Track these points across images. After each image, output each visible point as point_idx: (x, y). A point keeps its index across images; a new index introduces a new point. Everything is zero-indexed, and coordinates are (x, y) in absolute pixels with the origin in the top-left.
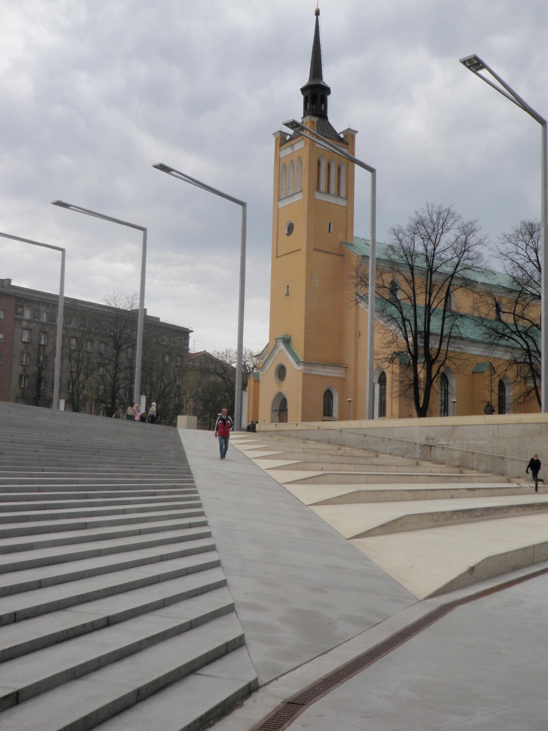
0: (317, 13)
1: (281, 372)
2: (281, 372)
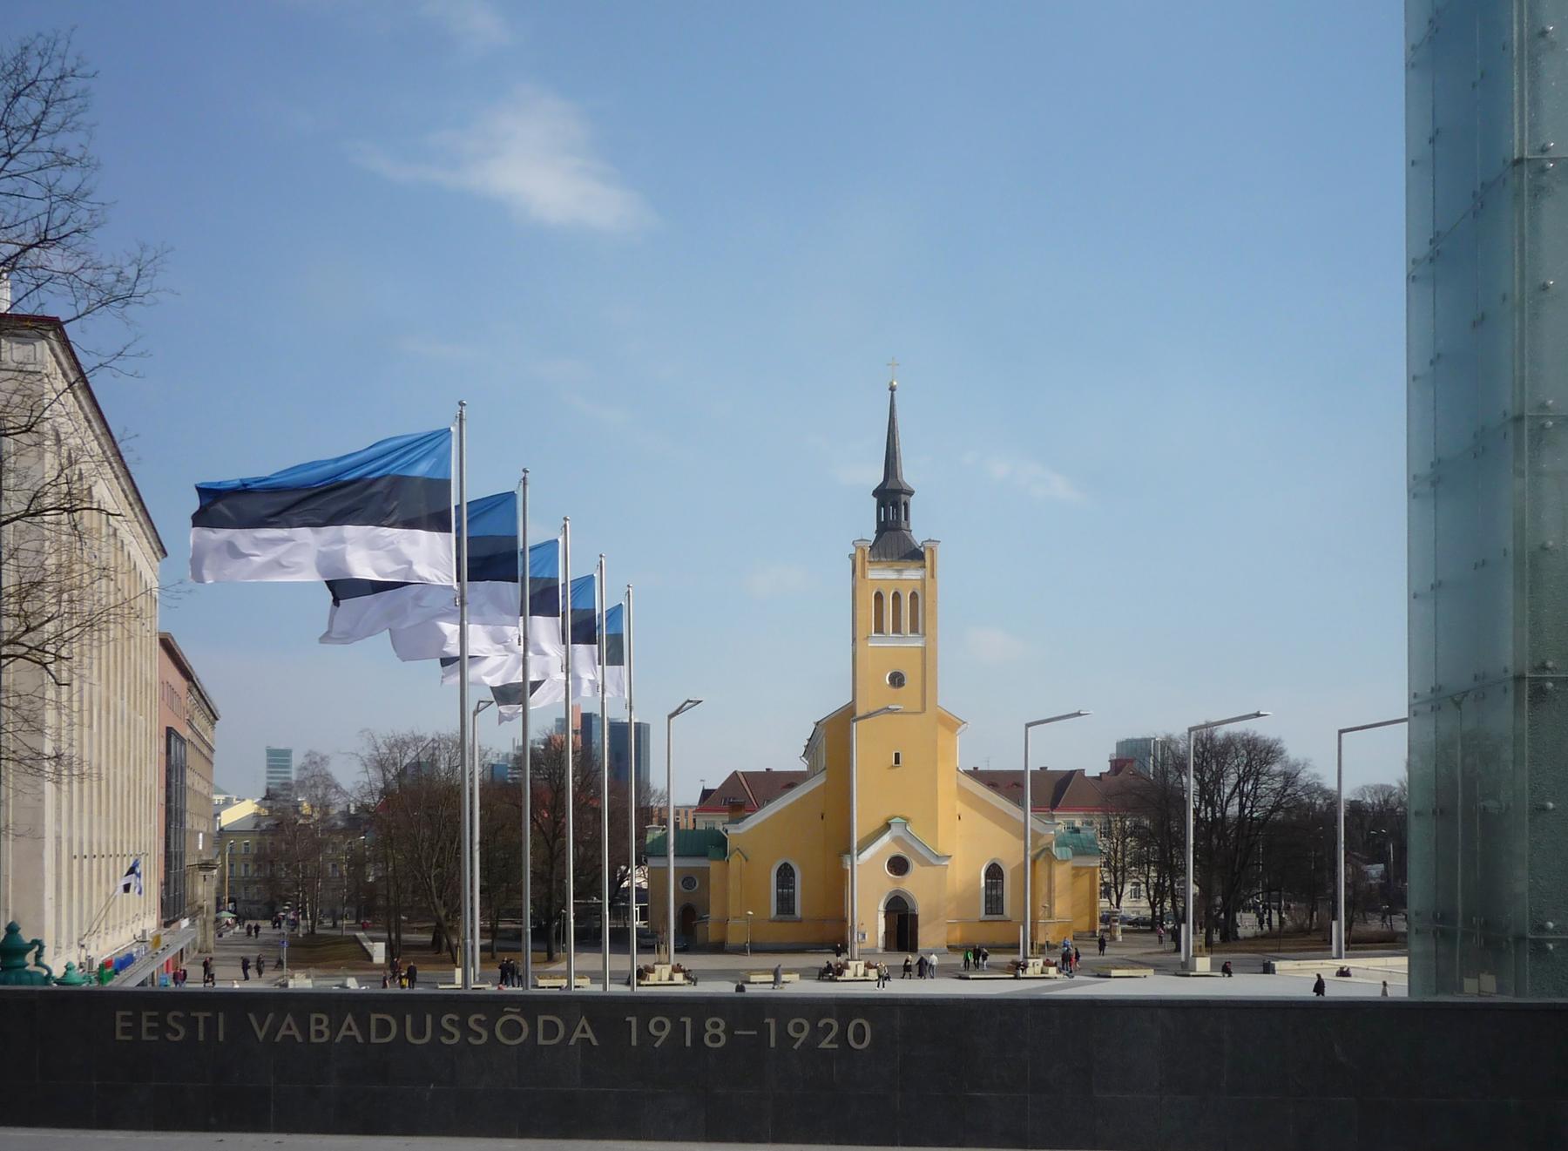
0: (892, 389)
2: (899, 866)
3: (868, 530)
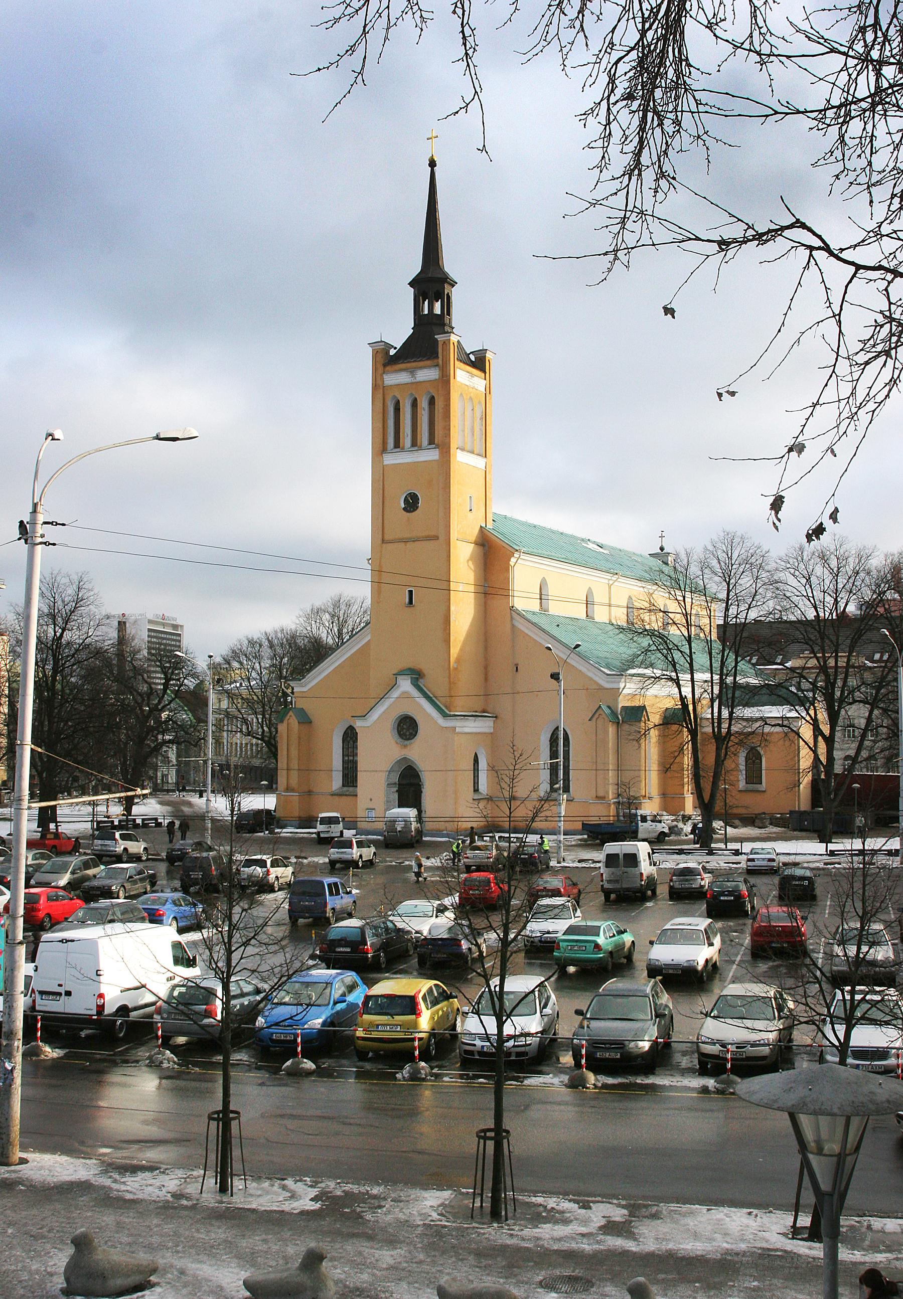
0: (432, 164)
1: (407, 727)
2: (407, 727)
3: (399, 330)
